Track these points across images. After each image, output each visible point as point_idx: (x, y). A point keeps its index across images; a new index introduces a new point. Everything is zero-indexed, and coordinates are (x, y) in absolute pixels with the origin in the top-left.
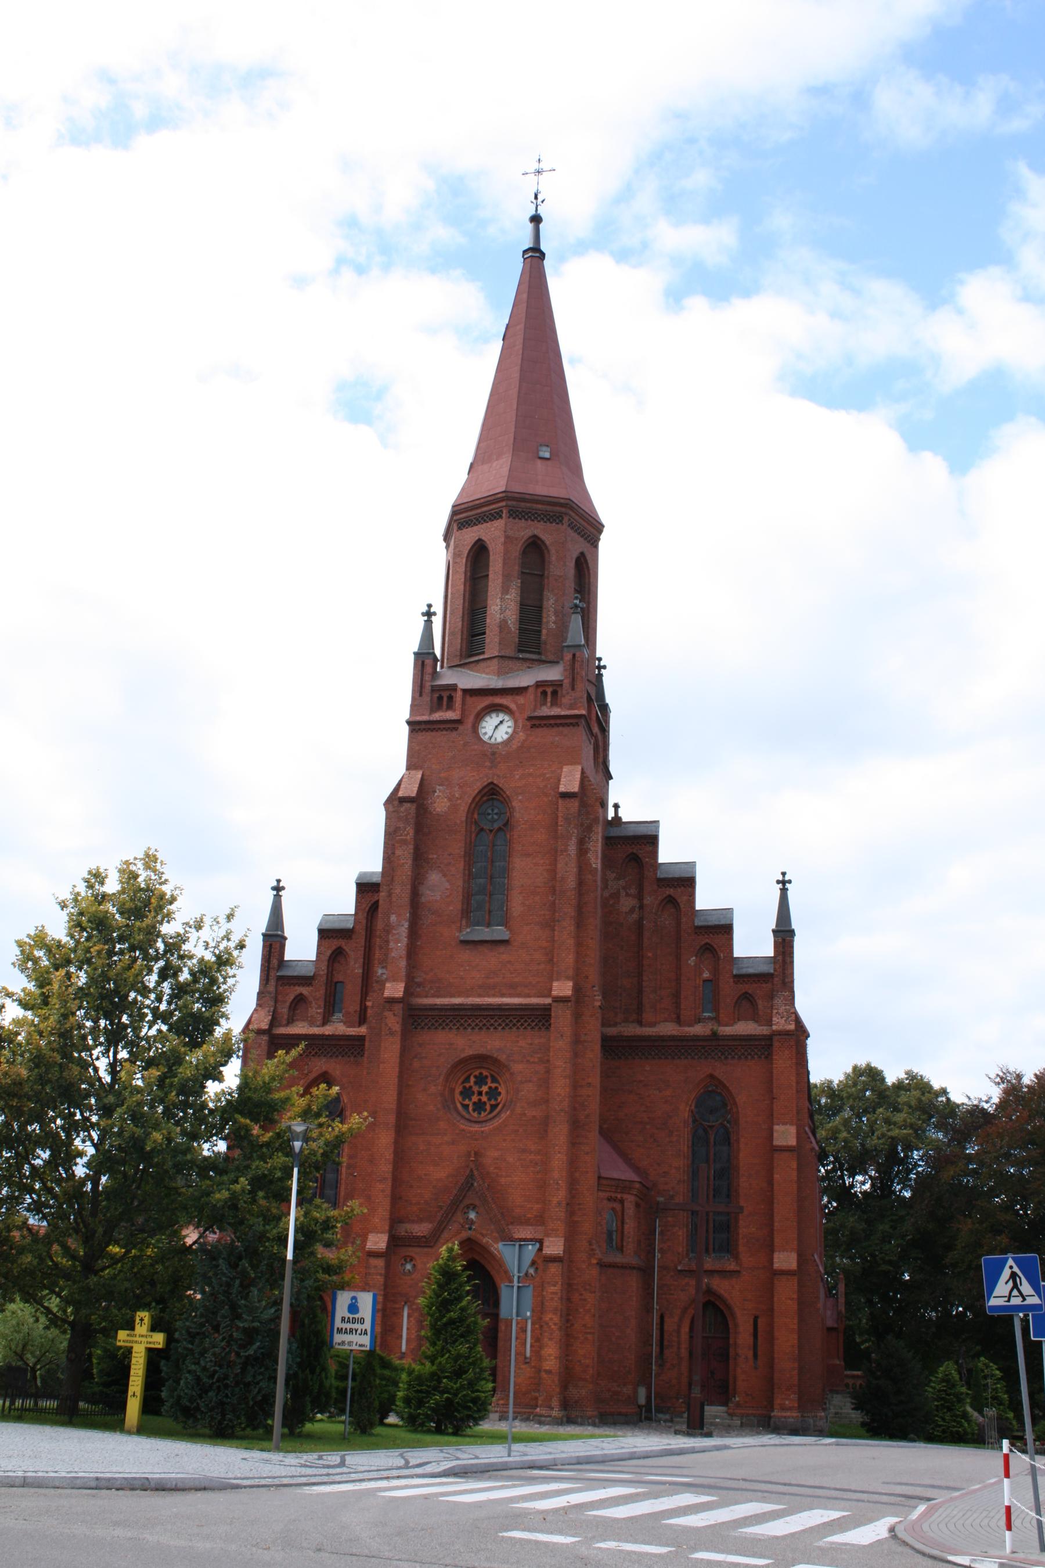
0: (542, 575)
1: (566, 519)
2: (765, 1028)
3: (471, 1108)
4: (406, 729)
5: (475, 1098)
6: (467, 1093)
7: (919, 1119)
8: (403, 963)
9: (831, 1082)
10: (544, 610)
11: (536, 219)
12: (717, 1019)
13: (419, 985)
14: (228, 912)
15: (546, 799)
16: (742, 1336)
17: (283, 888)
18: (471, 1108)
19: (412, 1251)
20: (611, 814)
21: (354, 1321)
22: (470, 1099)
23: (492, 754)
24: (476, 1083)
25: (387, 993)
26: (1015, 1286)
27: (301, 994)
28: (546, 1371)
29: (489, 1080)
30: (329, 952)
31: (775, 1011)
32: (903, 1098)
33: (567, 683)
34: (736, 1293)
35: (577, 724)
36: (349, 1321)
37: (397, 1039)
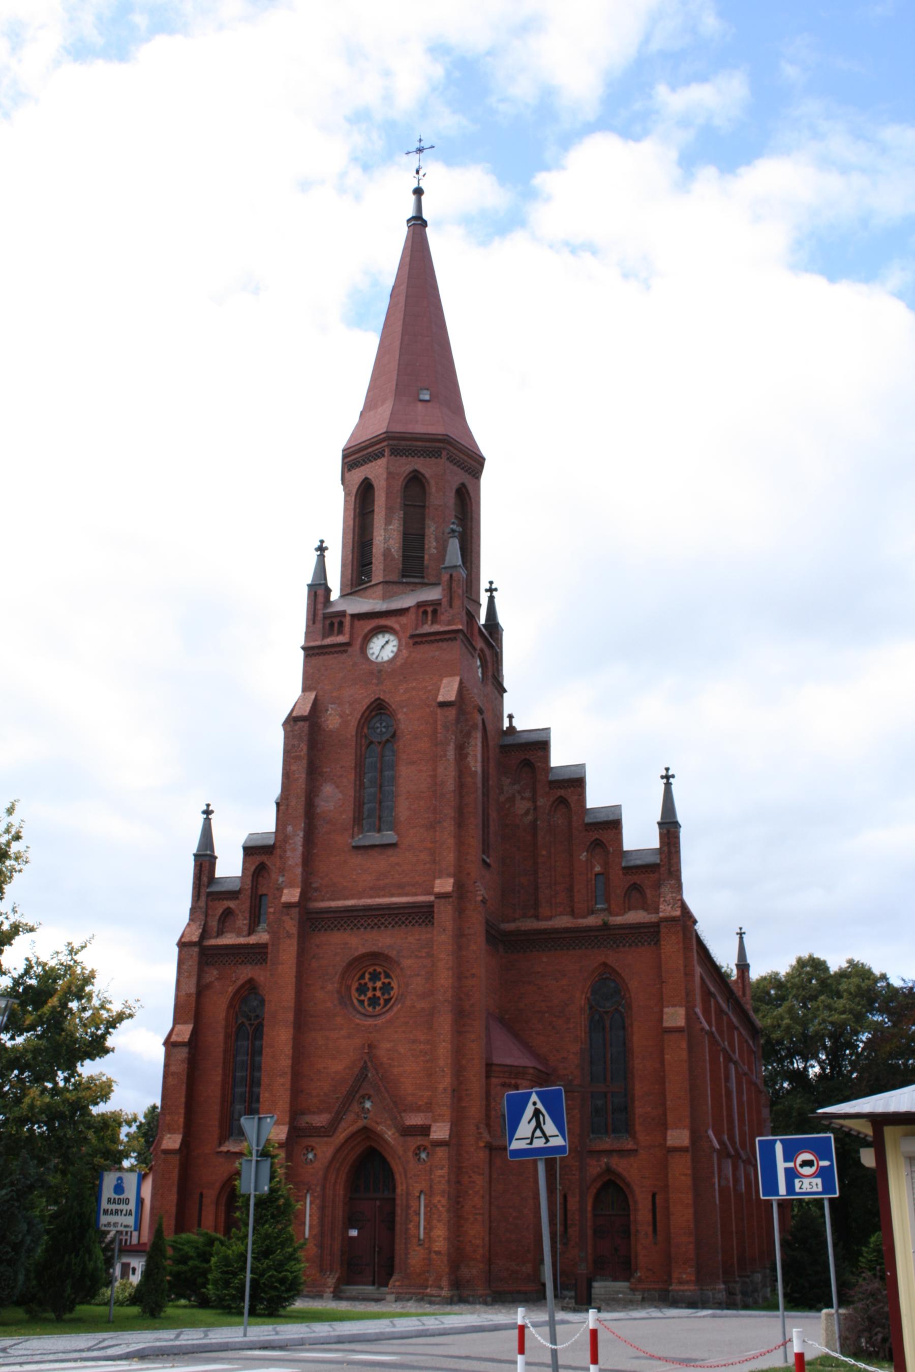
0: (424, 507)
1: (444, 453)
2: (653, 915)
3: (366, 1003)
4: (301, 653)
5: (370, 994)
6: (362, 989)
7: (858, 1004)
8: (299, 870)
9: (777, 974)
10: (426, 538)
11: (418, 192)
12: (609, 911)
13: (316, 890)
14: (9, 805)
15: (428, 710)
16: (642, 1214)
17: (212, 812)
18: (366, 1003)
19: (313, 1141)
20: (506, 724)
21: (120, 1201)
22: (365, 995)
23: (379, 671)
24: (370, 979)
25: (284, 899)
26: (539, 1126)
27: (229, 908)
28: (435, 1252)
29: (382, 976)
30: (253, 868)
31: (662, 899)
32: (843, 987)
33: (445, 602)
34: (635, 1172)
35: (455, 639)
36: (114, 1202)
37: (294, 942)
